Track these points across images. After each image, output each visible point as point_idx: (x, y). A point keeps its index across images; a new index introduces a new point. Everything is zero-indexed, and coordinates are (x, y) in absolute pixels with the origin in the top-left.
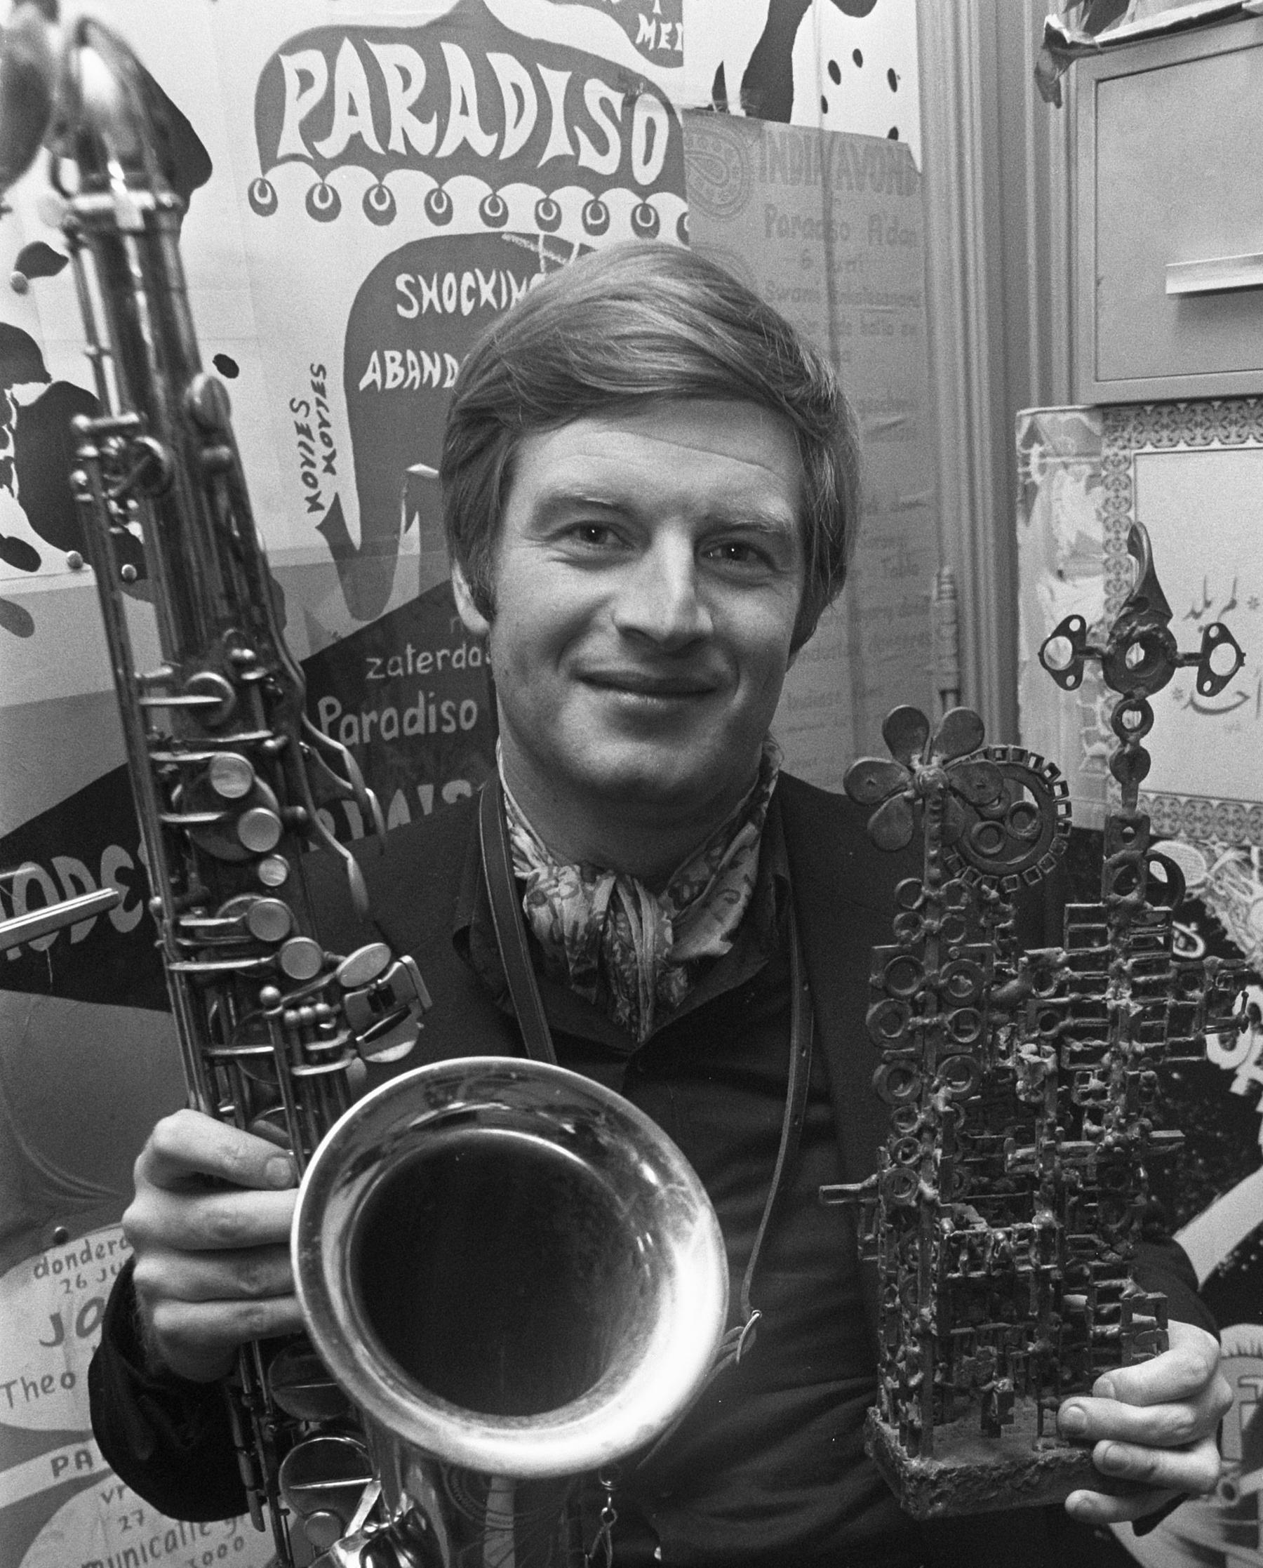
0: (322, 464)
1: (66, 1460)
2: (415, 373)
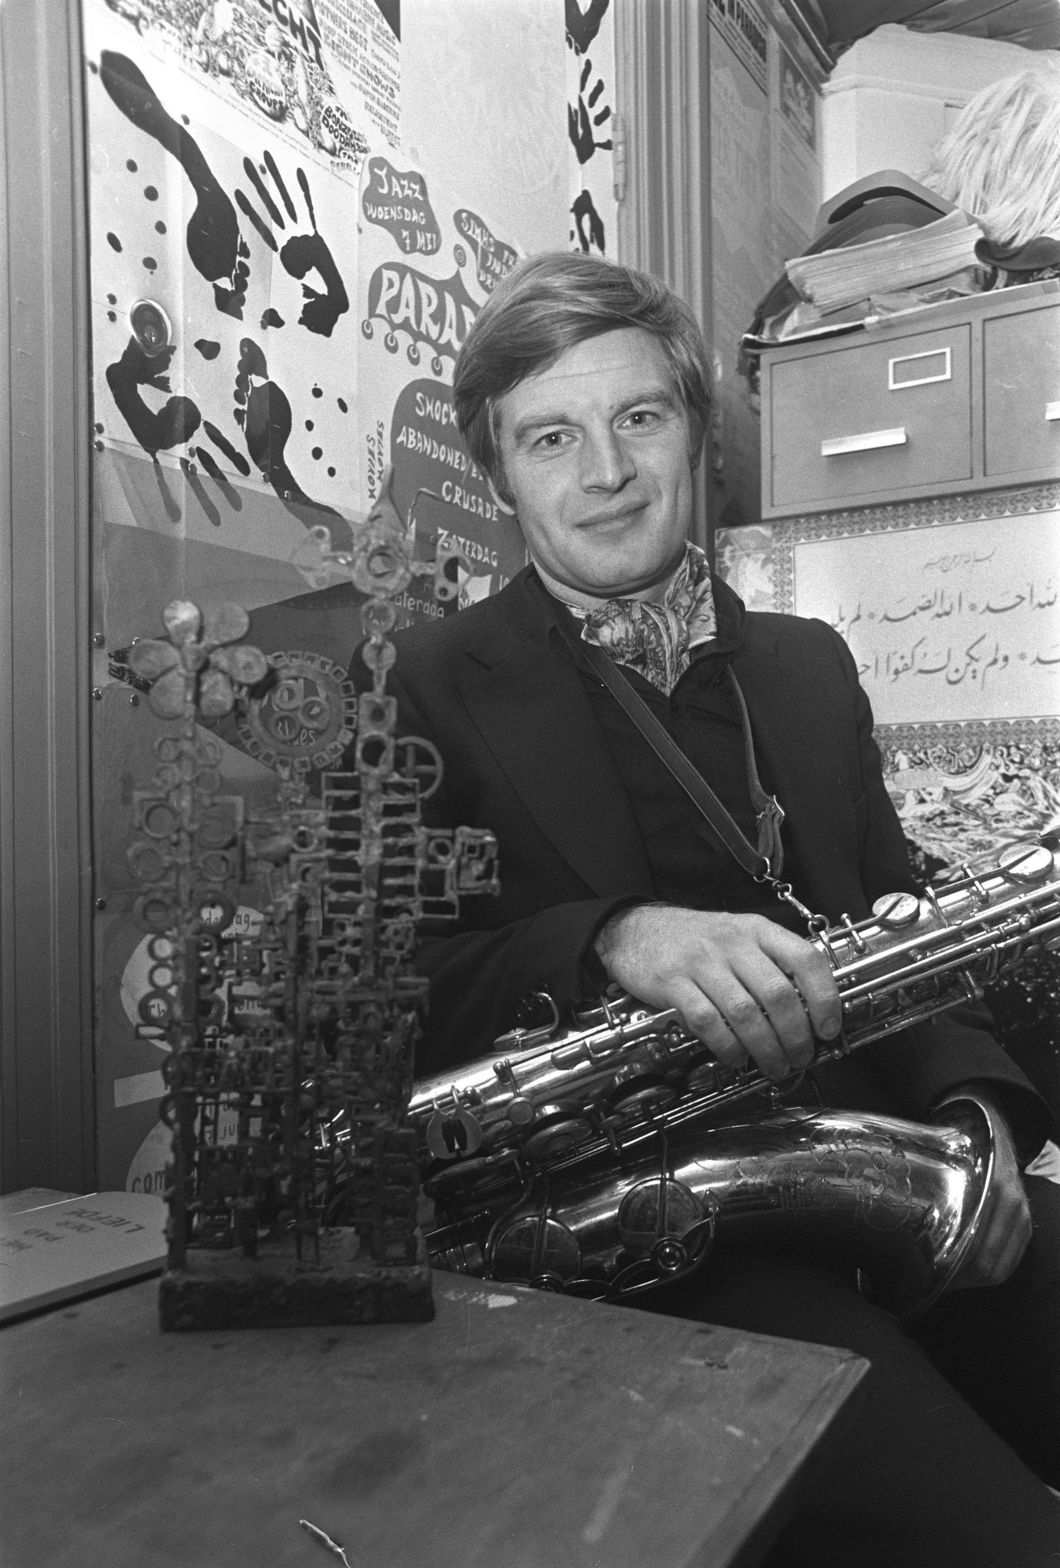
0: (377, 475)
2: (420, 445)
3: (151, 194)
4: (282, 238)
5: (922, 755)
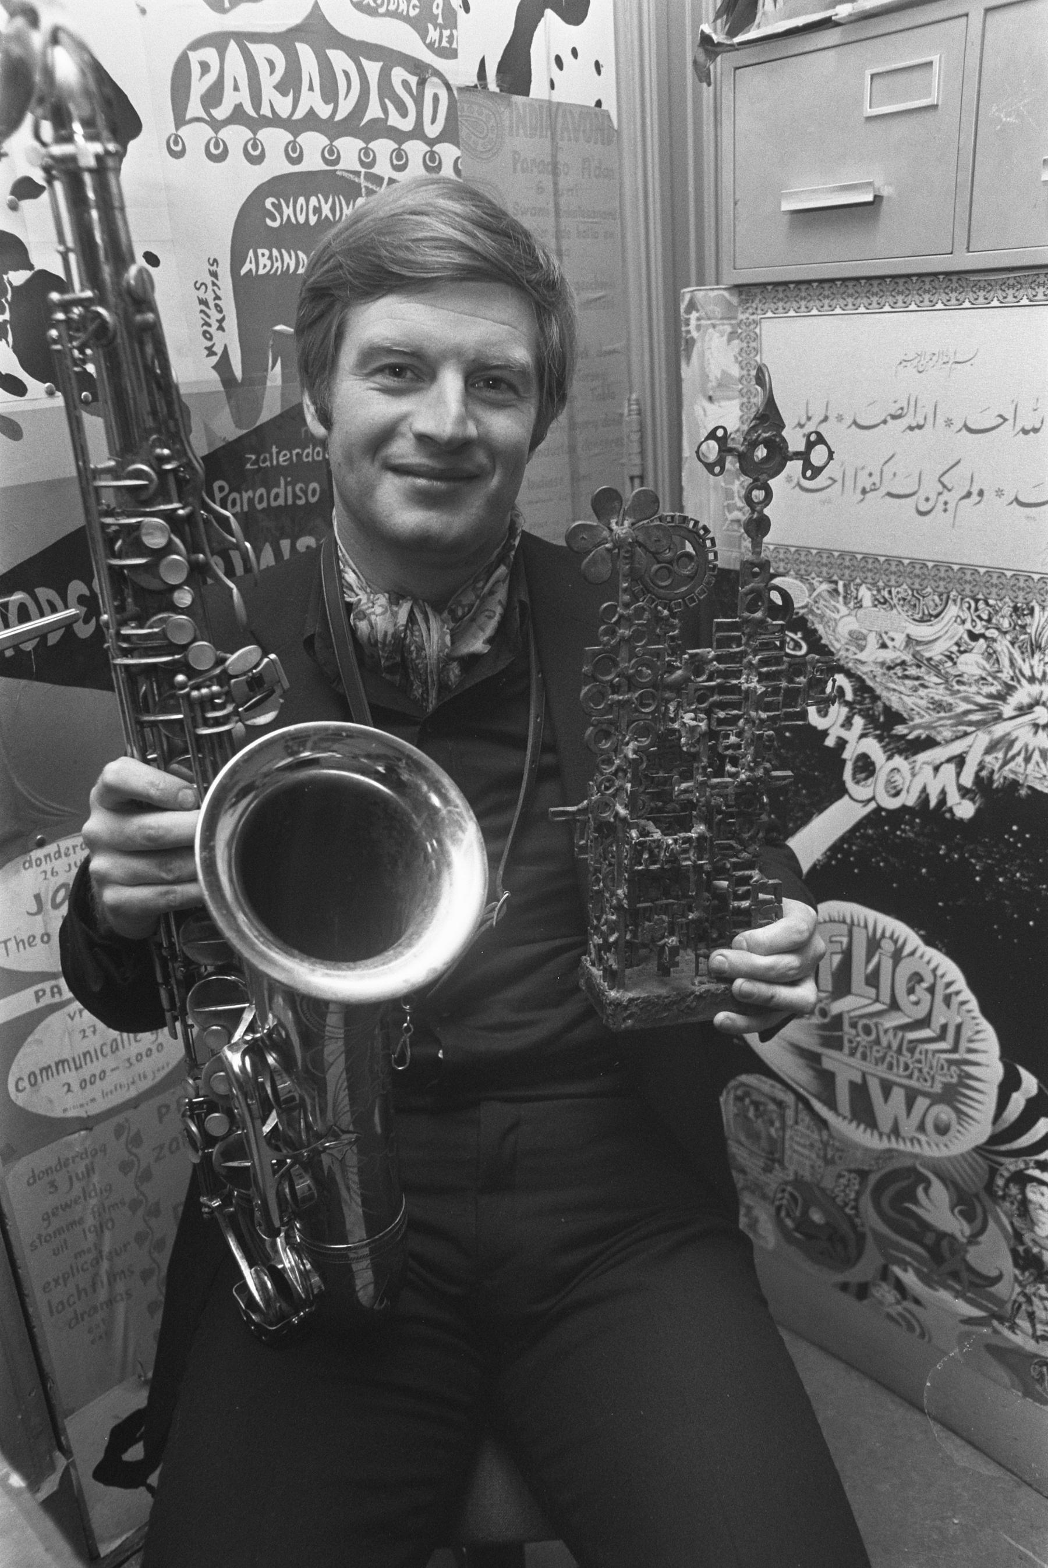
0: (215, 325)
5: (887, 596)
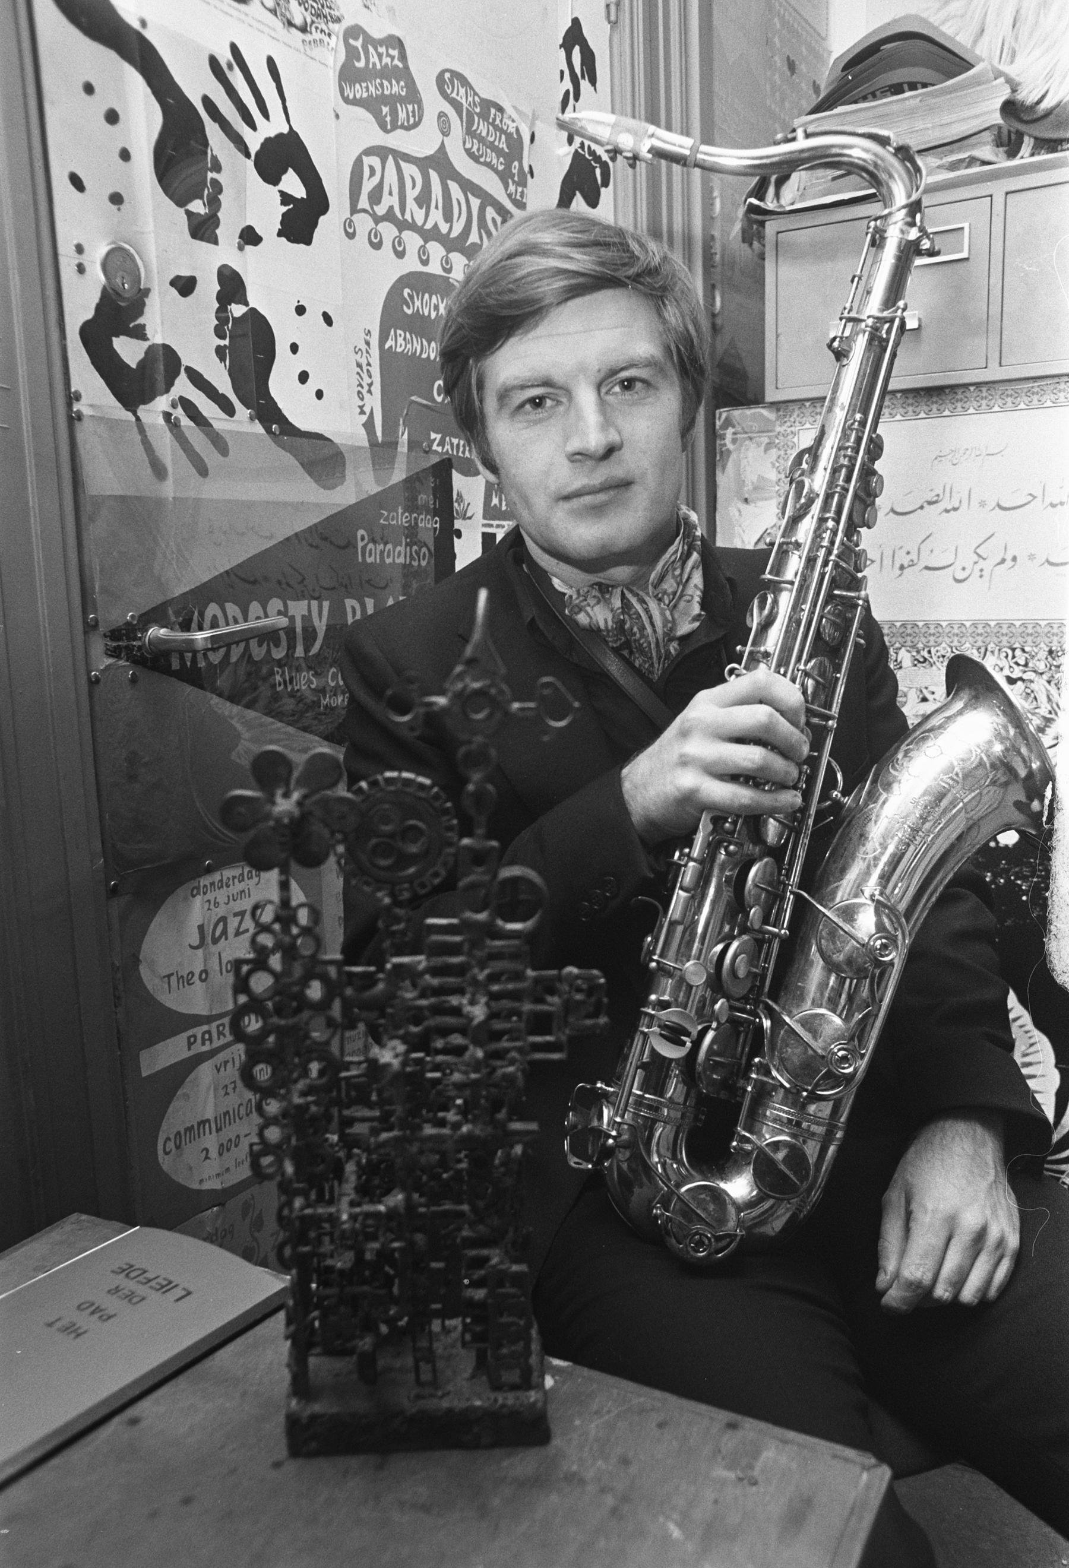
0: (366, 388)
1: (195, 1036)
2: (409, 346)
3: (112, 117)
4: (254, 141)
5: (925, 654)
